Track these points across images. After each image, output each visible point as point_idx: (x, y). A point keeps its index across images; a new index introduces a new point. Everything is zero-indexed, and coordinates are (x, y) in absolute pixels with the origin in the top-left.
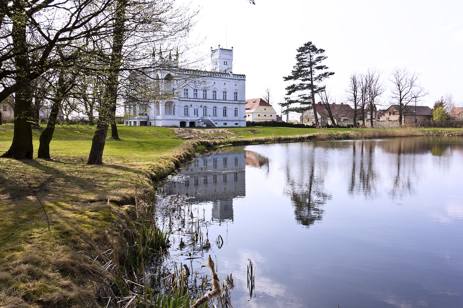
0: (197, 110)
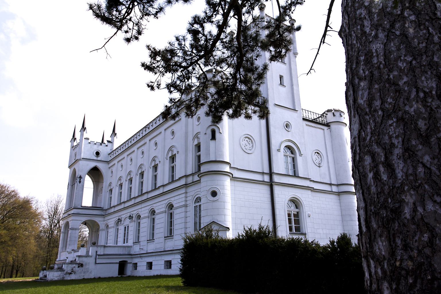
0: (128, 226)
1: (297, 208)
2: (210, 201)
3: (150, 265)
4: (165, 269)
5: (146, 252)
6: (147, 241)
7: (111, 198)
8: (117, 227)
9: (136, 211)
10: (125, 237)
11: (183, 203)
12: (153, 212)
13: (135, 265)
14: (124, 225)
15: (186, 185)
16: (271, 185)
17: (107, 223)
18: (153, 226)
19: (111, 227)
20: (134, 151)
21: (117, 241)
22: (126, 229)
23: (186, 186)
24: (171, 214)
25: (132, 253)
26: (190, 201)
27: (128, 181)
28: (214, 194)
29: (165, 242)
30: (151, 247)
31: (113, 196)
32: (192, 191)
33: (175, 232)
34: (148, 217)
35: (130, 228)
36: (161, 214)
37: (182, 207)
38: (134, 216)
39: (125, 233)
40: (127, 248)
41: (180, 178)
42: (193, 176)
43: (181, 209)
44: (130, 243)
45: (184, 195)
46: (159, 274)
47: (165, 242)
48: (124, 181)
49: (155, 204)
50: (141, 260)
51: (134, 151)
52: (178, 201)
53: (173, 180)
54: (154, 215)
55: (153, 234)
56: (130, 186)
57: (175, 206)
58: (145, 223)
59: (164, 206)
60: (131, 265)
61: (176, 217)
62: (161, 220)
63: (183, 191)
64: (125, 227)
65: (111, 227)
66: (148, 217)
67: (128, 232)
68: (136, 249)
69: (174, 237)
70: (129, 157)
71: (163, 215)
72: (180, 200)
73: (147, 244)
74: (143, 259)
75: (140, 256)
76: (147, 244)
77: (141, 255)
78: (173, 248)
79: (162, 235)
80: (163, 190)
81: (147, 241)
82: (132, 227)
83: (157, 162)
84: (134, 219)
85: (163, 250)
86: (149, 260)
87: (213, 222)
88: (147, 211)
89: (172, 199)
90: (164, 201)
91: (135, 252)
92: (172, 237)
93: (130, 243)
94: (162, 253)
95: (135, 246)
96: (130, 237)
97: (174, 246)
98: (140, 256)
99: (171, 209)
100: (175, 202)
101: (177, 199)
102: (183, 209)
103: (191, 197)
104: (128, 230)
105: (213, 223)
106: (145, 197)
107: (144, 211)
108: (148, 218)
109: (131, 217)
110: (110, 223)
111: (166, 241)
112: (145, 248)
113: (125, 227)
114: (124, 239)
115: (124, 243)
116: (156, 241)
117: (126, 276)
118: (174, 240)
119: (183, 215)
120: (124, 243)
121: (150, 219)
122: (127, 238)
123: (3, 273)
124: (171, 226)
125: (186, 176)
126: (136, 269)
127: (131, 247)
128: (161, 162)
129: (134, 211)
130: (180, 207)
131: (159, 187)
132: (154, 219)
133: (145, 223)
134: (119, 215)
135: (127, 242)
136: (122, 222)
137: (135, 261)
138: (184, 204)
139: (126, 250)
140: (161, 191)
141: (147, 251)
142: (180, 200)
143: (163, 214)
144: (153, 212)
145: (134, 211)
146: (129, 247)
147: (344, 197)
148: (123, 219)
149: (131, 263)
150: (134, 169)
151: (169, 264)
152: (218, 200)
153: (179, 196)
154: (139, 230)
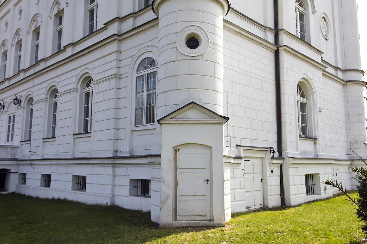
0: (14, 116)
1: (302, 96)
2: (185, 58)
3: (47, 180)
4: (73, 189)
5: (40, 158)
6: (21, 142)
7: (20, 57)
8: (30, 107)
9: (26, 92)
10: (9, 132)
11: (114, 71)
12: (54, 92)
13: (23, 177)
14: (7, 113)
15: (119, 37)
16: (227, 49)
17: (31, 93)
18: (55, 116)
19: (39, 101)
20: (9, 11)
21: (30, 131)
22: (12, 119)
23: (120, 38)
24: (87, 94)
25: (18, 157)
26: (128, 67)
27: (14, 47)
28: (193, 42)
29: (74, 142)
30: (50, 150)
31: (22, 53)
32: (134, 48)
33: (95, 127)
34: (46, 100)
35: (17, 119)
36: (69, 95)
37: (109, 79)
38: (23, 99)
39: (9, 126)
40: (9, 149)
41: (107, 25)
42: (135, 18)
43: (107, 83)
44: (16, 141)
45: (114, 56)
46: (62, 197)
47: (74, 142)
48: (10, 45)
49: (93, 63)
50: (32, 170)
51: (9, 11)
52: (101, 69)
53: (92, 32)
54: (56, 96)
55: (54, 128)
56: (19, 54)
57: (95, 78)
58: (41, 111)
59: (74, 79)
60: (17, 176)
61: (96, 99)
62: (69, 106)
63: (113, 47)
64: (10, 117)
65: (39, 101)
66: (46, 100)
67: (13, 125)
68: (24, 152)
69: (92, 135)
70: (18, 7)
71: (73, 95)
72: (107, 67)
73: (44, 146)
74: (36, 167)
75: (31, 162)
76: (44, 146)
77: (32, 162)
78: (90, 154)
79: (71, 131)
80: (134, 23)
81: (43, 139)
82: (21, 115)
83: (63, 6)
84: (22, 104)
85: (70, 157)
86: (47, 171)
87: (193, 103)
88: (44, 91)
89: (91, 66)
90: (74, 71)
91: (23, 156)
92: (89, 135)
93: (16, 141)
94: (69, 162)
95: (23, 146)
96: (16, 132)
97: (91, 152)
98: (31, 162)
99: (88, 85)
100: (61, 84)
101: (99, 65)
102: (114, 81)
103: (75, 78)
104: (14, 122)
105: (191, 106)
106: (42, 66)
107: (38, 89)
108: (44, 102)
109: (17, 101)
110: (35, 94)
111: (77, 140)
112: (39, 151)
113: (10, 117)
114: (8, 135)
115: (8, 141)
116: (95, 135)
117: (6, 193)
118: (91, 139)
119: (112, 94)
120: (8, 141)
121: (48, 103)
122: (12, 134)
123: (177, 120)
124: (87, 115)
125: (120, 19)
126: (24, 182)
127: (17, 147)
128: (69, 5)
129: (21, 91)
130: (40, 102)
131: (66, 47)
132: (55, 104)
133: (41, 111)
134: (15, 93)
135: (12, 140)
136: (5, 109)
137: (24, 169)
138: (115, 72)
139: (7, 152)
140: (69, 52)
141: (42, 156)
142: (107, 67)
143: (72, 94)
144: (54, 92)
145: (21, 91)
146: (12, 147)
147: (352, 88)
148: (6, 105)
149: (17, 172)
150: (24, 25)
151: (80, 181)
152: (202, 55)
153: (104, 59)
154: (31, 121)
